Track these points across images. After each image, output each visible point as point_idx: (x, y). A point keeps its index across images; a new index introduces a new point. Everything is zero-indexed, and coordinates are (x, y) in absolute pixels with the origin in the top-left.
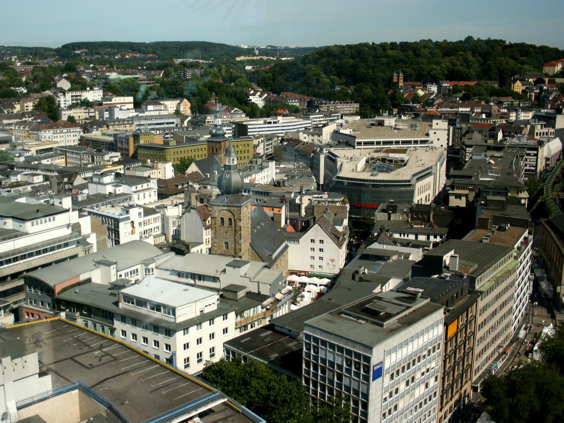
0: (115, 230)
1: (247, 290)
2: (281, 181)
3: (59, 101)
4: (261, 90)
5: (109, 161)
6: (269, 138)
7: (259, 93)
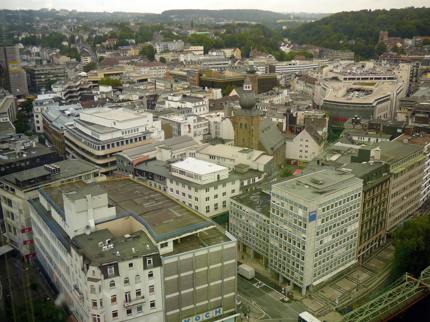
3: (156, 49)
4: (290, 42)
5: (181, 87)
7: (287, 45)
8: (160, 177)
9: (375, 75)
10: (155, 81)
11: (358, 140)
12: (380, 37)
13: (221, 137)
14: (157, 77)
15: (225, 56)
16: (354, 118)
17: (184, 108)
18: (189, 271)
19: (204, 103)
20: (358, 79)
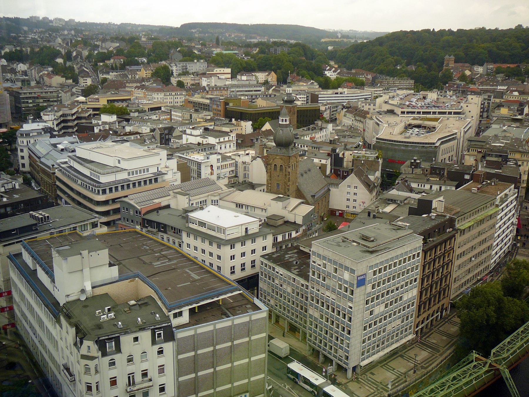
1: (286, 219)
3: (172, 70)
4: (336, 66)
7: (334, 69)
9: (439, 109)
11: (417, 187)
14: (172, 105)
15: (258, 81)
16: (413, 161)
17: (206, 144)
18: (208, 347)
19: (231, 138)
20: (419, 113)
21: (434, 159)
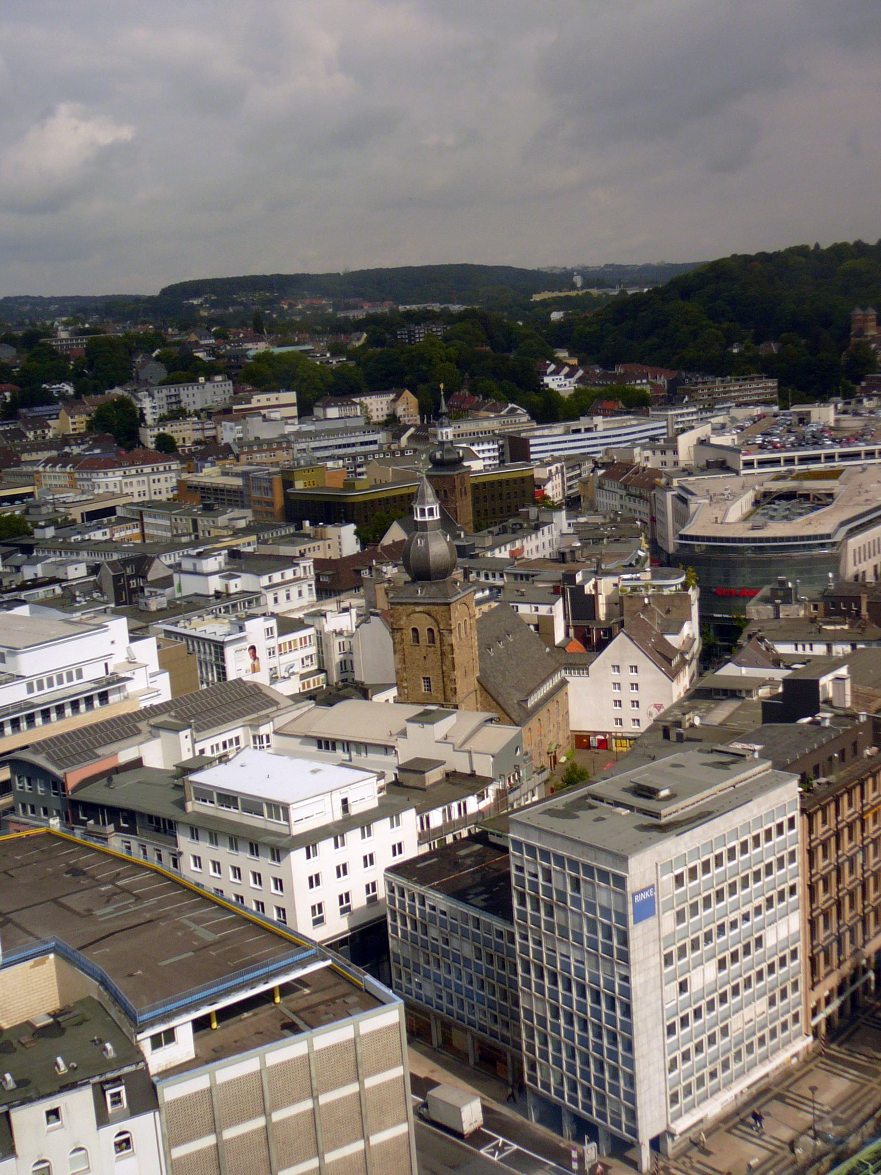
0: (218, 666)
1: (448, 767)
2: (567, 550)
3: (141, 409)
4: (574, 361)
5: (226, 527)
6: (571, 463)
7: (566, 370)
8: (158, 823)
10: (141, 513)
11: (794, 652)
12: (855, 327)
13: (357, 678)
14: (147, 498)
15: (368, 418)
17: (236, 593)
18: (250, 1118)
19: (300, 573)
20: (789, 461)
21: (831, 575)
